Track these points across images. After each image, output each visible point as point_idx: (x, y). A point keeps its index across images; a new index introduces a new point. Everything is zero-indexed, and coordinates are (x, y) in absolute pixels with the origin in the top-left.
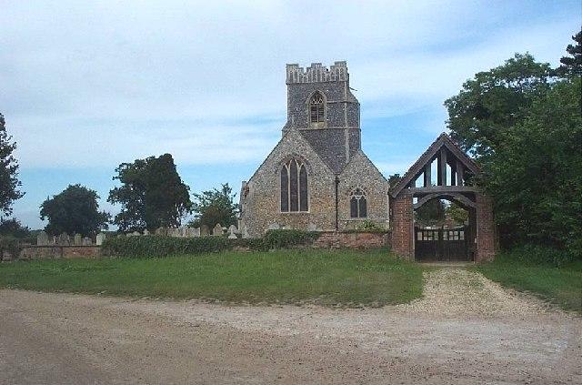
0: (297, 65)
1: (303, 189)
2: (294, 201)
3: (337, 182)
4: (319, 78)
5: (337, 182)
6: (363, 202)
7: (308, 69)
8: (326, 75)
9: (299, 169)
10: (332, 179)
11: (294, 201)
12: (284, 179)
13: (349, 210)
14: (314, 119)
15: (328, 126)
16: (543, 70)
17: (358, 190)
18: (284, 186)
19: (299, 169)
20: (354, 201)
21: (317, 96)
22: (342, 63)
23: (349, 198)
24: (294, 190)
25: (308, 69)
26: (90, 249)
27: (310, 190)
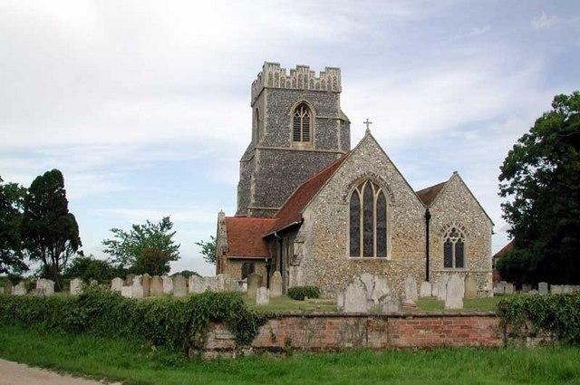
0: (278, 65)
1: (381, 225)
2: (368, 241)
3: (428, 216)
4: (300, 85)
5: (428, 216)
6: (460, 246)
7: (292, 71)
8: (315, 82)
9: (376, 196)
10: (421, 213)
11: (368, 241)
12: (354, 208)
13: (442, 256)
14: (297, 138)
15: (317, 147)
16: (26, 190)
17: (454, 230)
18: (354, 220)
19: (376, 196)
20: (448, 246)
21: (303, 107)
22: (337, 69)
23: (442, 241)
24: (368, 227)
25: (292, 71)
26: (466, 321)
27: (390, 226)
